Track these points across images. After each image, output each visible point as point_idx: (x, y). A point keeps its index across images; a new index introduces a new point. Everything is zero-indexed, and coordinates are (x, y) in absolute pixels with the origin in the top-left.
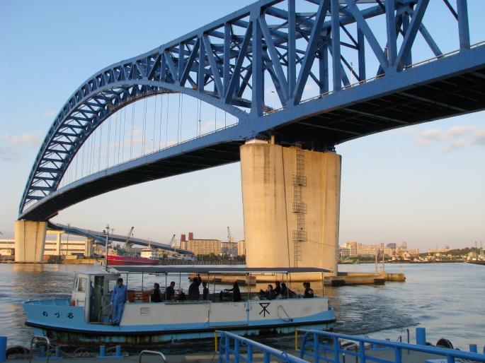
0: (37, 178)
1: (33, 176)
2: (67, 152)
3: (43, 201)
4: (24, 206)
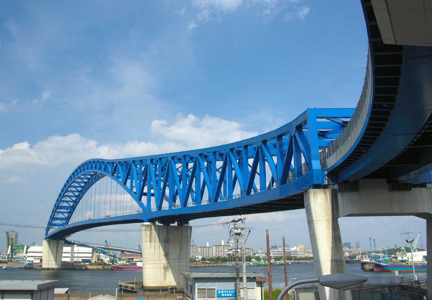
1: (54, 212)
4: (49, 230)
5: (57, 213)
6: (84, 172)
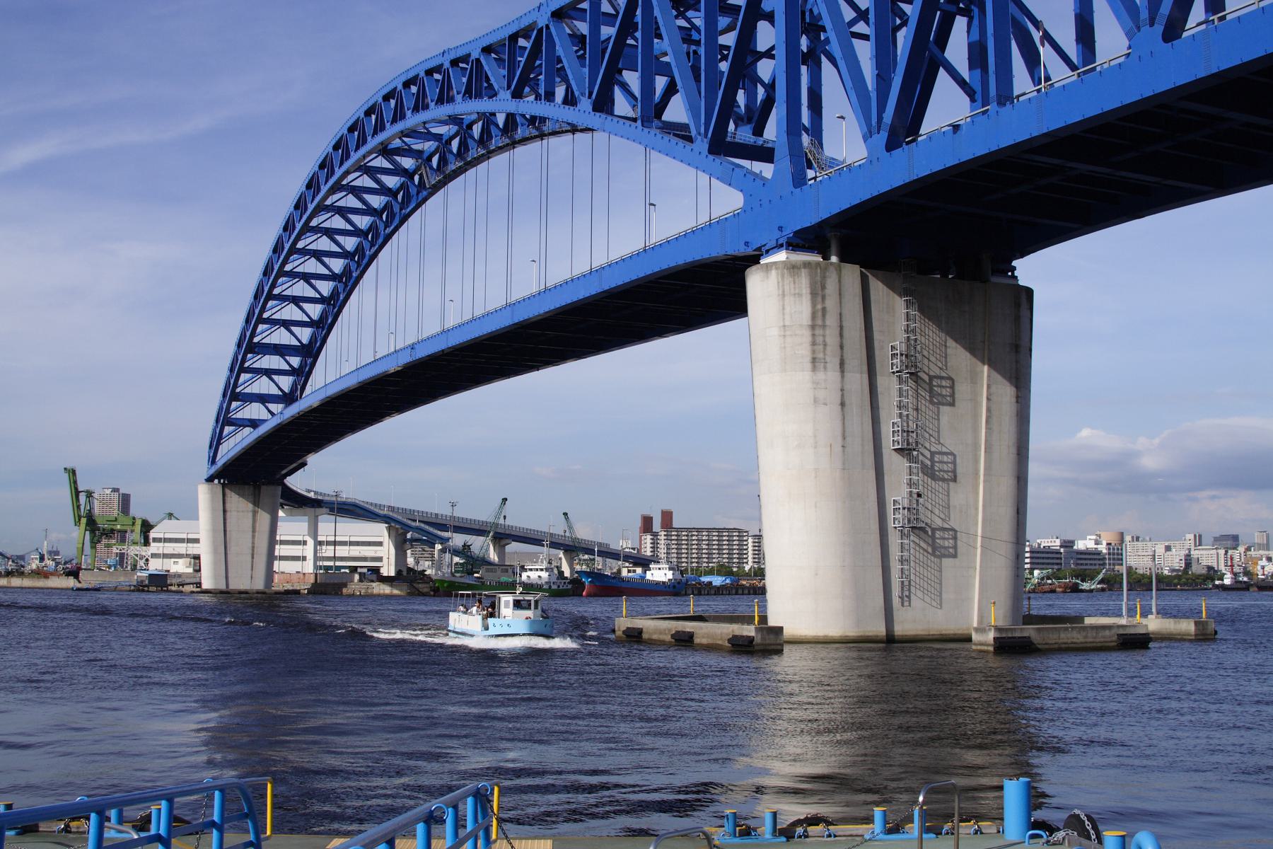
0: (249, 370)
1: (238, 367)
2: (322, 300)
3: (262, 430)
4: (219, 444)
5: (275, 302)
6: (381, 137)
